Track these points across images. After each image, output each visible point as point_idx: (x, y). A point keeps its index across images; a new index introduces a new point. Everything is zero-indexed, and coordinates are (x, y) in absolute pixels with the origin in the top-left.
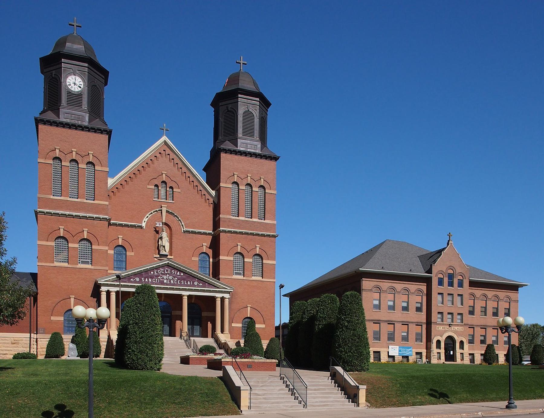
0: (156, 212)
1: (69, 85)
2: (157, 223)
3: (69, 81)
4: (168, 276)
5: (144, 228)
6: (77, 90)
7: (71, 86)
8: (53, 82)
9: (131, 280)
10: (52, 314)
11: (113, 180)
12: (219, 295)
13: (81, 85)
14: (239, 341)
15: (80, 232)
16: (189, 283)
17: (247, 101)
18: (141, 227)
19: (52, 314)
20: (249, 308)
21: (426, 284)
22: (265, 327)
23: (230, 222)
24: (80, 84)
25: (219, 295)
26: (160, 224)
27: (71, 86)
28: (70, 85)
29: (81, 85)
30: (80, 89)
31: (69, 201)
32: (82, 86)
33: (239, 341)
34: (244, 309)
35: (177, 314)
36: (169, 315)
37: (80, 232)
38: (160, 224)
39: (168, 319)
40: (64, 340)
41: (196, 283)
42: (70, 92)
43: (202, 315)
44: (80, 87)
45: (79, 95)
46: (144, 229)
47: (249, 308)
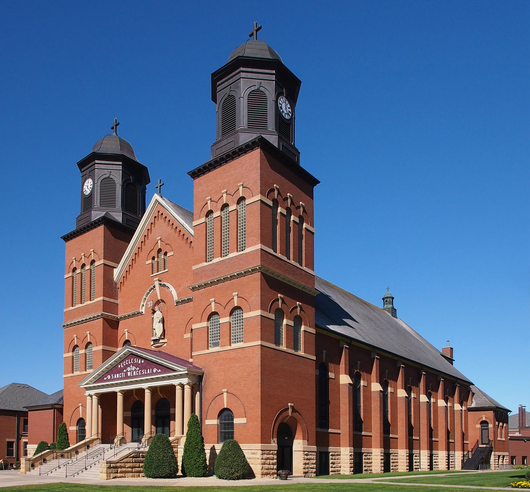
0: (153, 290)
5: (144, 313)
8: (130, 203)
9: (105, 379)
10: (70, 425)
11: (117, 269)
12: (176, 382)
14: (214, 446)
16: (148, 372)
18: (139, 313)
19: (70, 425)
20: (225, 395)
21: (121, 163)
22: (246, 422)
23: (203, 271)
25: (176, 382)
31: (80, 308)
33: (214, 446)
34: (220, 396)
41: (155, 371)
43: (171, 413)
46: (144, 314)
47: (225, 395)
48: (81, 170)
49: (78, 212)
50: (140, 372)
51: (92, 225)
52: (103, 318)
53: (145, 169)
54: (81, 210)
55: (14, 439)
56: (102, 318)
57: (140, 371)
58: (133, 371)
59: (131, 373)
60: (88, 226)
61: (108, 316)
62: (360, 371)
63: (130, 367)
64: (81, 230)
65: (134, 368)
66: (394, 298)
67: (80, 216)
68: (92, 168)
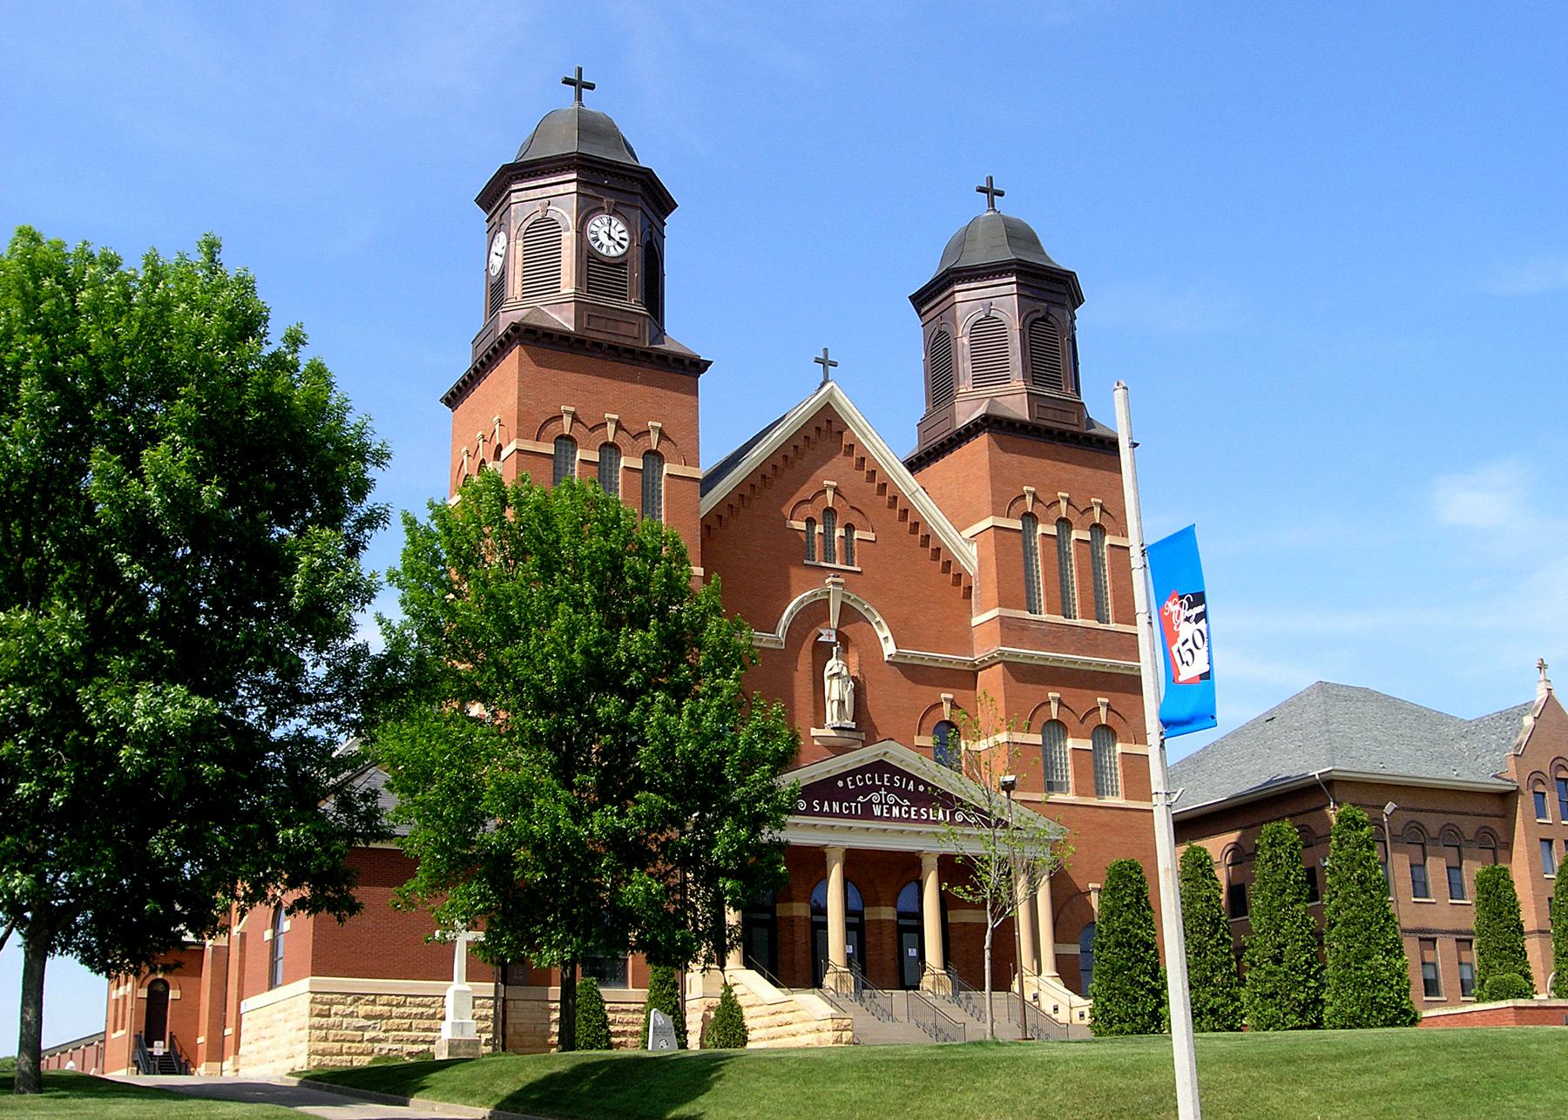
1: (594, 239)
2: (822, 631)
3: (594, 228)
4: (883, 792)
6: (613, 253)
7: (598, 243)
13: (625, 240)
15: (1426, 811)
17: (1001, 291)
24: (621, 239)
26: (829, 635)
27: (598, 243)
28: (596, 240)
29: (625, 240)
30: (621, 251)
32: (625, 244)
35: (883, 917)
36: (768, 916)
37: (1426, 811)
38: (829, 635)
39: (765, 932)
40: (745, 1012)
41: (959, 818)
42: (594, 258)
44: (623, 247)
45: (619, 264)
48: (919, 312)
49: (920, 408)
50: (913, 813)
51: (959, 434)
52: (1004, 662)
53: (1070, 276)
54: (927, 404)
55: (553, 974)
56: (999, 663)
57: (913, 809)
58: (891, 806)
59: (885, 811)
60: (950, 440)
61: (1011, 654)
62: (166, 978)
63: (881, 795)
64: (928, 454)
65: (892, 798)
66: (913, 298)
67: (926, 416)
68: (505, 205)
